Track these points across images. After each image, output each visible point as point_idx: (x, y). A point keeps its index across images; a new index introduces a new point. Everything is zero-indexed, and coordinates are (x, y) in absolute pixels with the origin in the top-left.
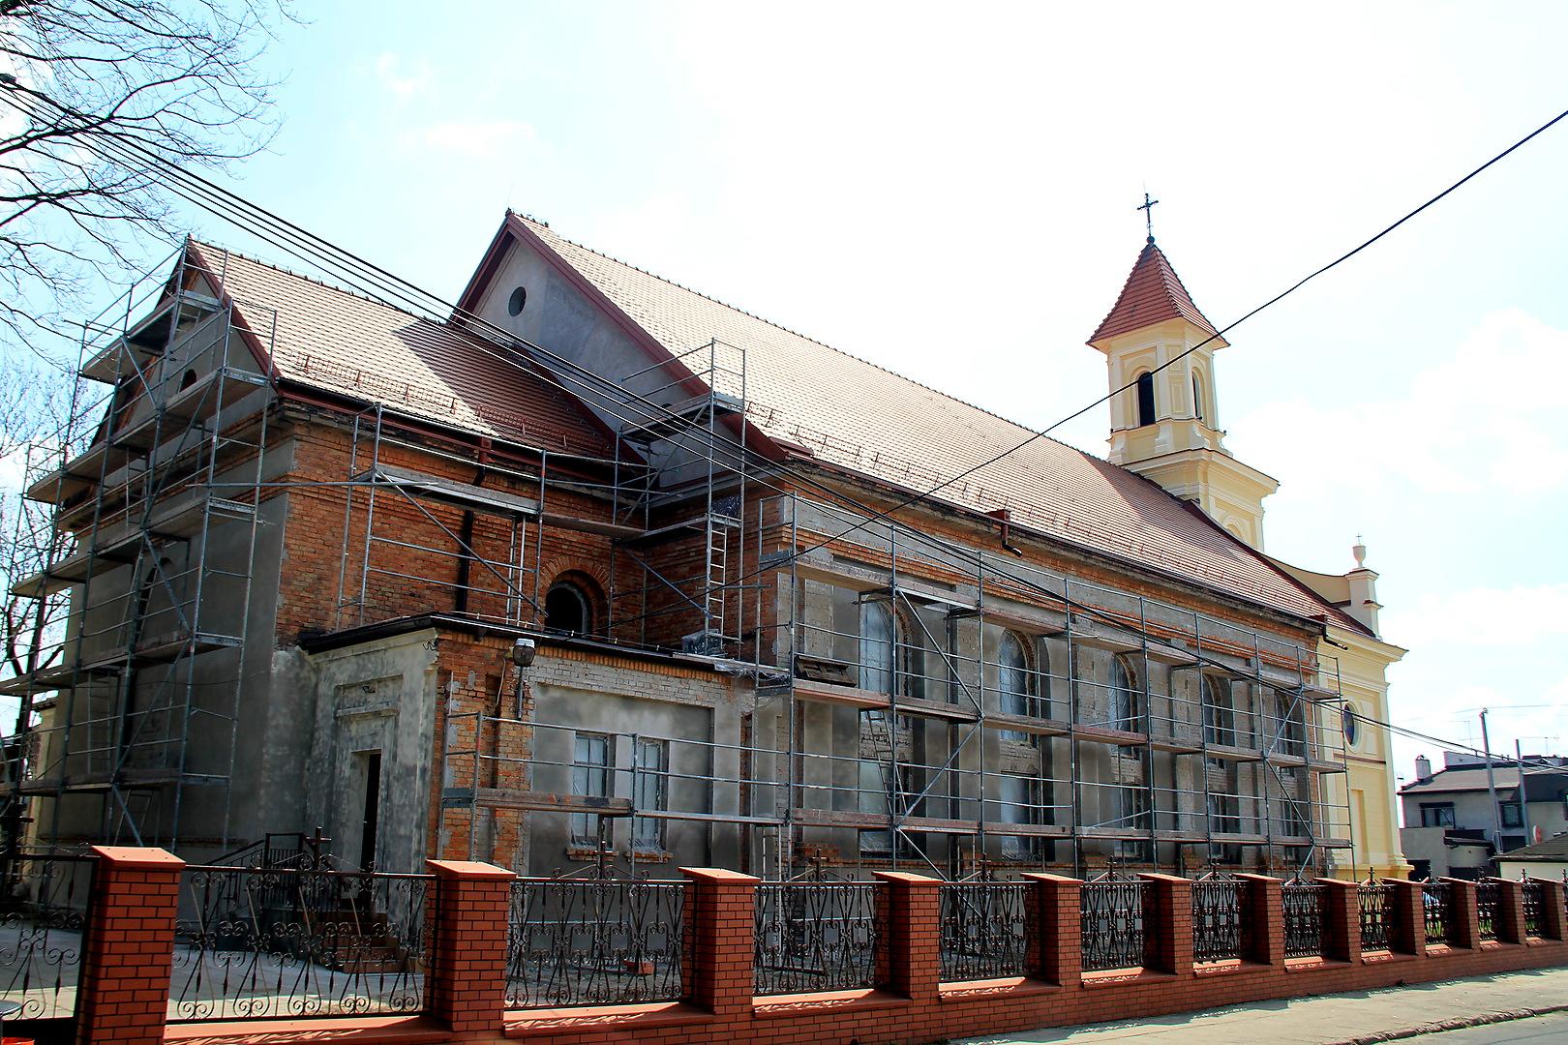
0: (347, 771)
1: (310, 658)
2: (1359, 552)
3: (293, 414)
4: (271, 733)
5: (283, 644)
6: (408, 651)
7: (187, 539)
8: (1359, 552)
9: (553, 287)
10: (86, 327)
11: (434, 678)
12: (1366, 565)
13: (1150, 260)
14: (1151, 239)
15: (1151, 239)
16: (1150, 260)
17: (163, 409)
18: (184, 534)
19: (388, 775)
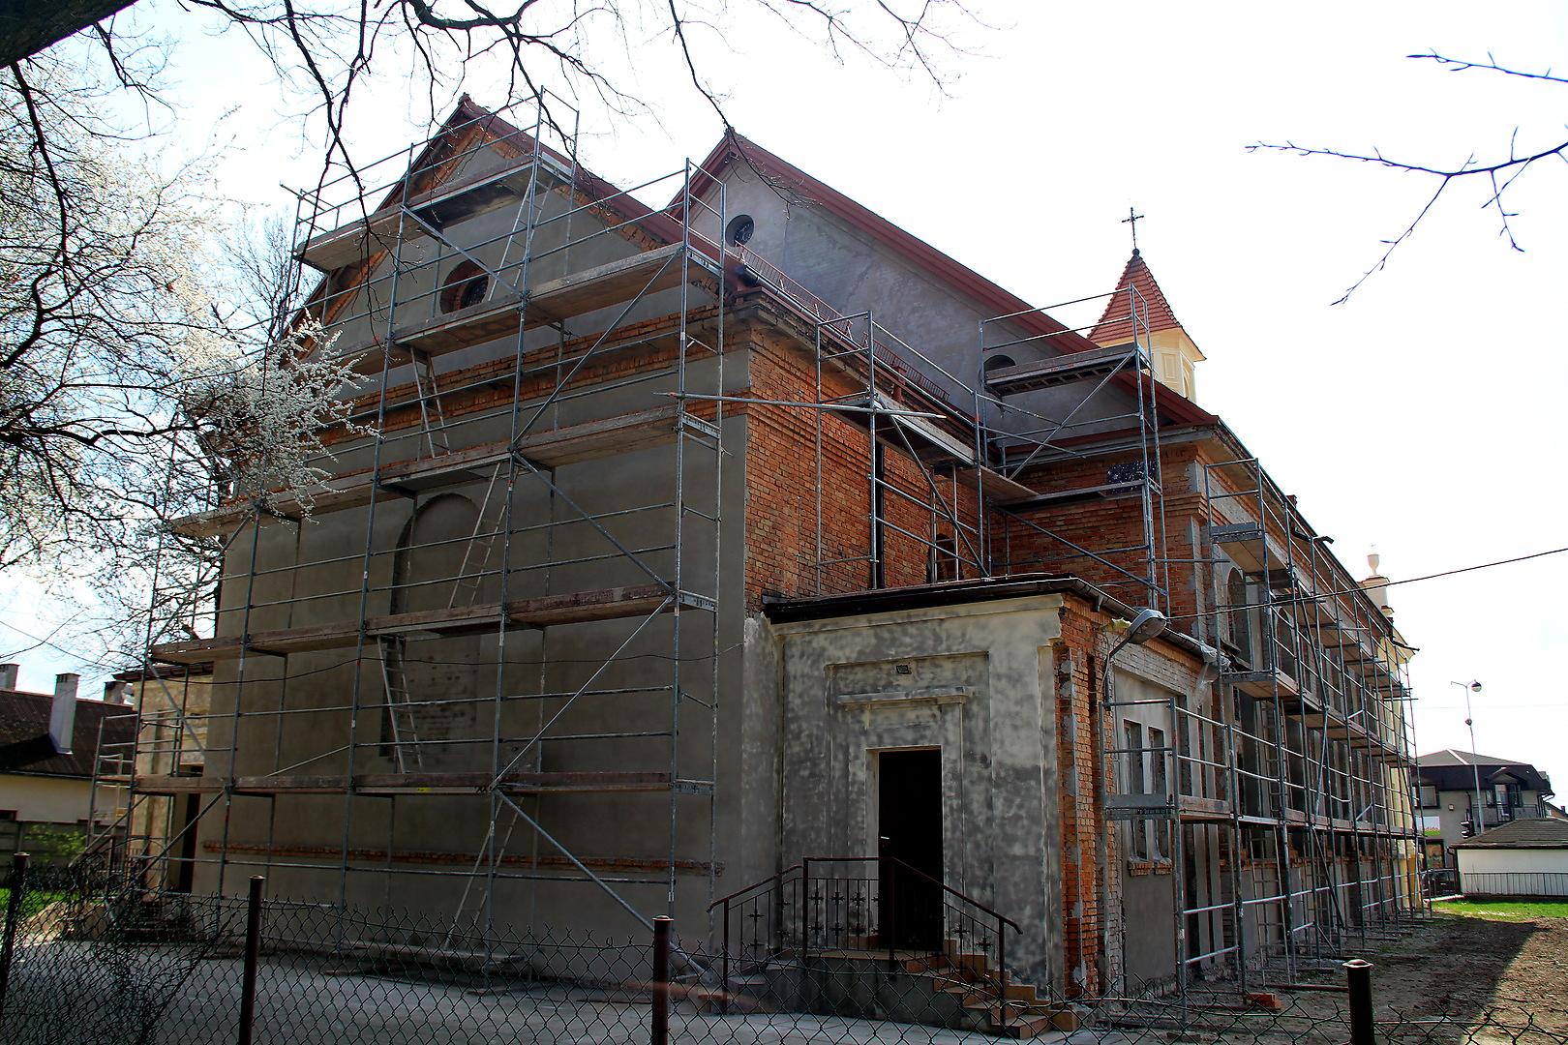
0: (862, 775)
1: (772, 628)
2: (1373, 560)
3: (764, 315)
4: (746, 726)
5: (751, 613)
6: (995, 622)
7: (551, 469)
8: (1373, 560)
9: (799, 218)
10: (301, 198)
11: (1049, 657)
12: (1380, 572)
13: (1136, 268)
14: (1136, 252)
15: (1136, 252)
16: (1136, 268)
17: (527, 296)
18: (551, 463)
19: (957, 776)
